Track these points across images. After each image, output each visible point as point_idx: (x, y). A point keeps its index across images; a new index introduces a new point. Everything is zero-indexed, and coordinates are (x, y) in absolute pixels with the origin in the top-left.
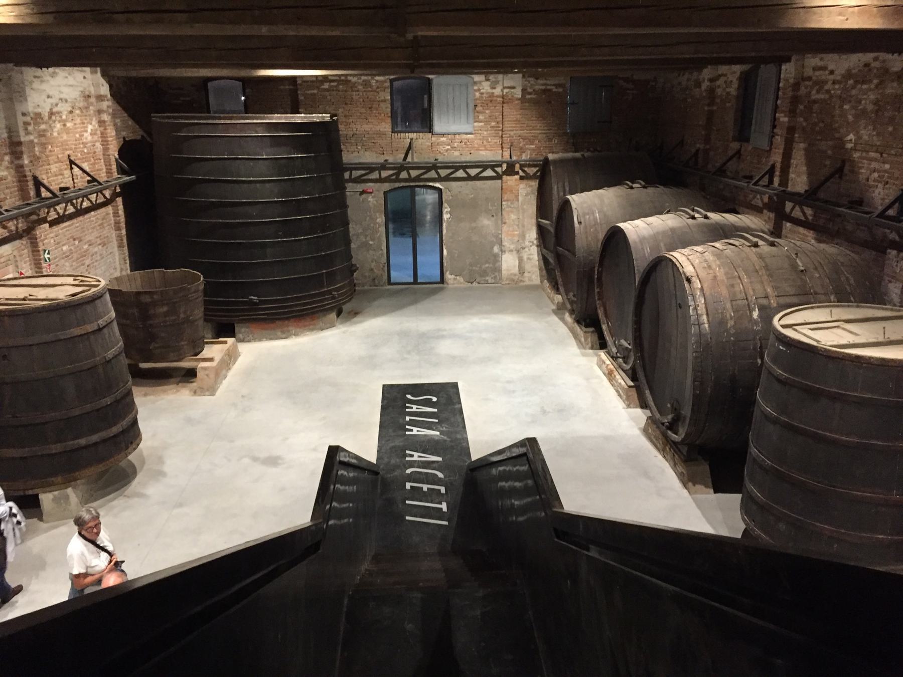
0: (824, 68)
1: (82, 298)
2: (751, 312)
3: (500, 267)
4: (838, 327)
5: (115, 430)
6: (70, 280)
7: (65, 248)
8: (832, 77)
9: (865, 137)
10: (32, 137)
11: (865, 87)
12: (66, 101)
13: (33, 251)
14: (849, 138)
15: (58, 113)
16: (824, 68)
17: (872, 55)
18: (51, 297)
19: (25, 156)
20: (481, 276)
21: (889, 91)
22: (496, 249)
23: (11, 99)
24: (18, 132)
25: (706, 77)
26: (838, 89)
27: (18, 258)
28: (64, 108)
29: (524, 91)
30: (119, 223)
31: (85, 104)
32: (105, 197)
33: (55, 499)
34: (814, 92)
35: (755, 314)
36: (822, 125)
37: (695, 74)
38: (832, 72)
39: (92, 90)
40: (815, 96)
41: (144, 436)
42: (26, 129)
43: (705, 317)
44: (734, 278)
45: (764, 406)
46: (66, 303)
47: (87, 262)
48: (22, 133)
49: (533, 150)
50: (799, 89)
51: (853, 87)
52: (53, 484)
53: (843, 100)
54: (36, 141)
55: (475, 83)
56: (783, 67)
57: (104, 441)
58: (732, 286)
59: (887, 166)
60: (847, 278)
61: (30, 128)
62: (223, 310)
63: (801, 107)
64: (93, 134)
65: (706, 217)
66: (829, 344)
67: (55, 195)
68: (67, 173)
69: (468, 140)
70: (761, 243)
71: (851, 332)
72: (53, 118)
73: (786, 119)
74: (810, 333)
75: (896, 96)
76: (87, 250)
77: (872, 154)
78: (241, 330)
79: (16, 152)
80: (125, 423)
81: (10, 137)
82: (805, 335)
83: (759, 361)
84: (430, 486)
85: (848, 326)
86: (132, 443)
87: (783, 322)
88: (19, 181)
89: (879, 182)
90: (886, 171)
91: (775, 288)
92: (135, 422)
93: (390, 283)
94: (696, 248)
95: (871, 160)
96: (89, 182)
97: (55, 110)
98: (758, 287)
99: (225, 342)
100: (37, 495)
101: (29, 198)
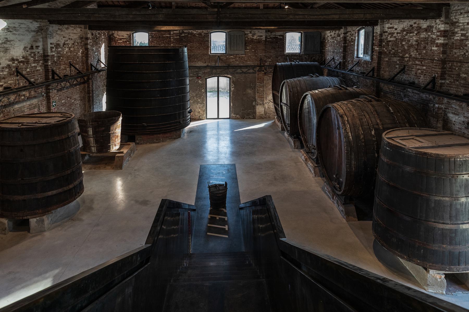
0: (393, 28)
1: (62, 123)
2: (371, 132)
3: (256, 111)
4: (413, 139)
5: (71, 186)
6: (59, 115)
7: (63, 101)
8: (396, 31)
9: (413, 55)
10: (54, 53)
11: (411, 35)
12: (72, 39)
13: (48, 102)
14: (406, 56)
15: (67, 44)
16: (393, 28)
17: (414, 21)
18: (48, 122)
19: (49, 61)
20: (247, 115)
21: (422, 36)
22: (254, 103)
23: (46, 37)
24: (48, 51)
25: (342, 32)
26: (400, 36)
27: (40, 106)
28: (70, 42)
29: (266, 37)
30: (90, 91)
31: (80, 41)
32: (84, 80)
33: (37, 221)
34: (389, 38)
35: (373, 133)
36: (393, 51)
37: (337, 31)
38: (396, 29)
39: (84, 35)
40: (389, 39)
41: (85, 190)
42: (51, 50)
43: (350, 134)
44: (362, 115)
45: (381, 177)
46: (54, 125)
47: (73, 108)
48: (49, 51)
49: (270, 61)
50: (382, 36)
51: (406, 35)
52: (35, 214)
53: (402, 40)
54: (56, 55)
55: (245, 34)
56: (375, 28)
57: (65, 192)
58: (362, 119)
59: (424, 68)
60: (413, 116)
61: (54, 50)
62: (166, 127)
63: (384, 44)
64: (82, 53)
65: (346, 89)
66: (410, 146)
67: (61, 78)
68: (68, 69)
69: (242, 57)
70: (372, 100)
71: (419, 141)
72: (65, 46)
73: (378, 49)
74: (400, 141)
75: (425, 38)
76: (73, 102)
77: (417, 62)
78: (138, 138)
79: (45, 60)
80: (77, 183)
81: (44, 53)
82: (398, 142)
83: (376, 155)
84: (220, 217)
85: (418, 138)
86: (78, 193)
87: (387, 136)
88: (45, 72)
89: (421, 74)
90: (424, 70)
91: (380, 120)
92: (81, 183)
93: (207, 119)
94: (344, 102)
95: (417, 65)
96: (78, 73)
97: (66, 43)
98: (373, 119)
99: (130, 144)
100: (28, 219)
101: (49, 79)
